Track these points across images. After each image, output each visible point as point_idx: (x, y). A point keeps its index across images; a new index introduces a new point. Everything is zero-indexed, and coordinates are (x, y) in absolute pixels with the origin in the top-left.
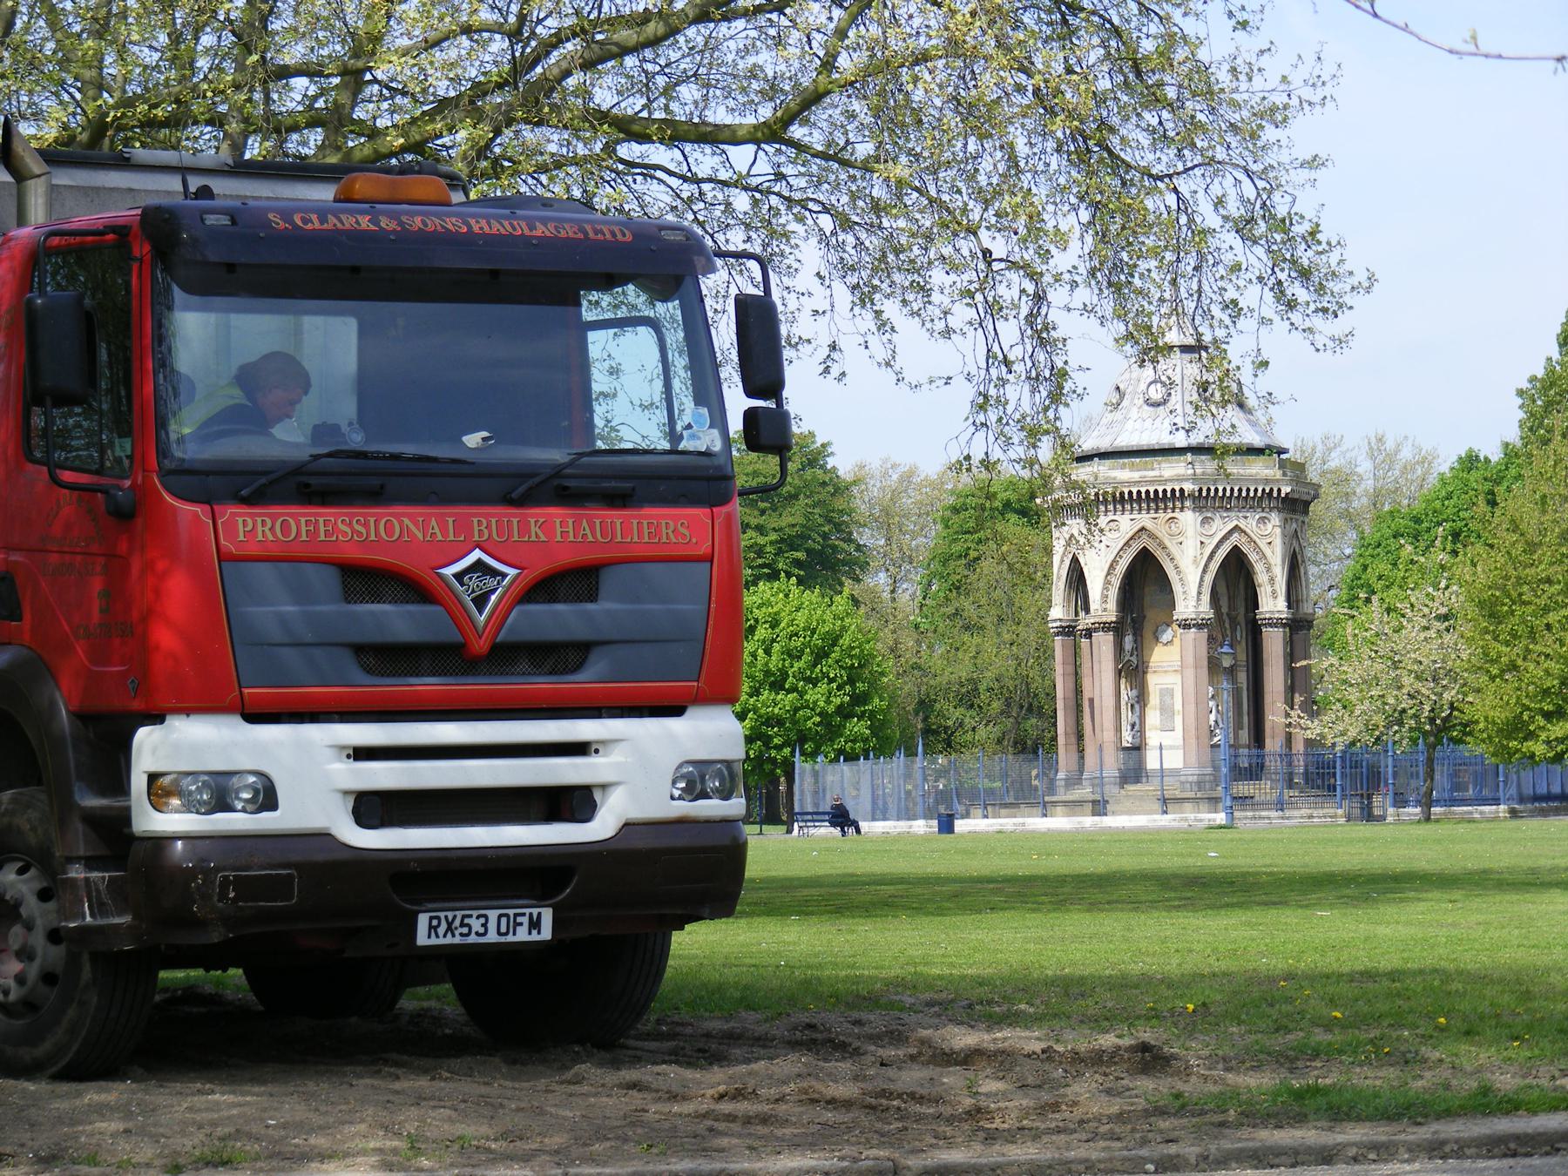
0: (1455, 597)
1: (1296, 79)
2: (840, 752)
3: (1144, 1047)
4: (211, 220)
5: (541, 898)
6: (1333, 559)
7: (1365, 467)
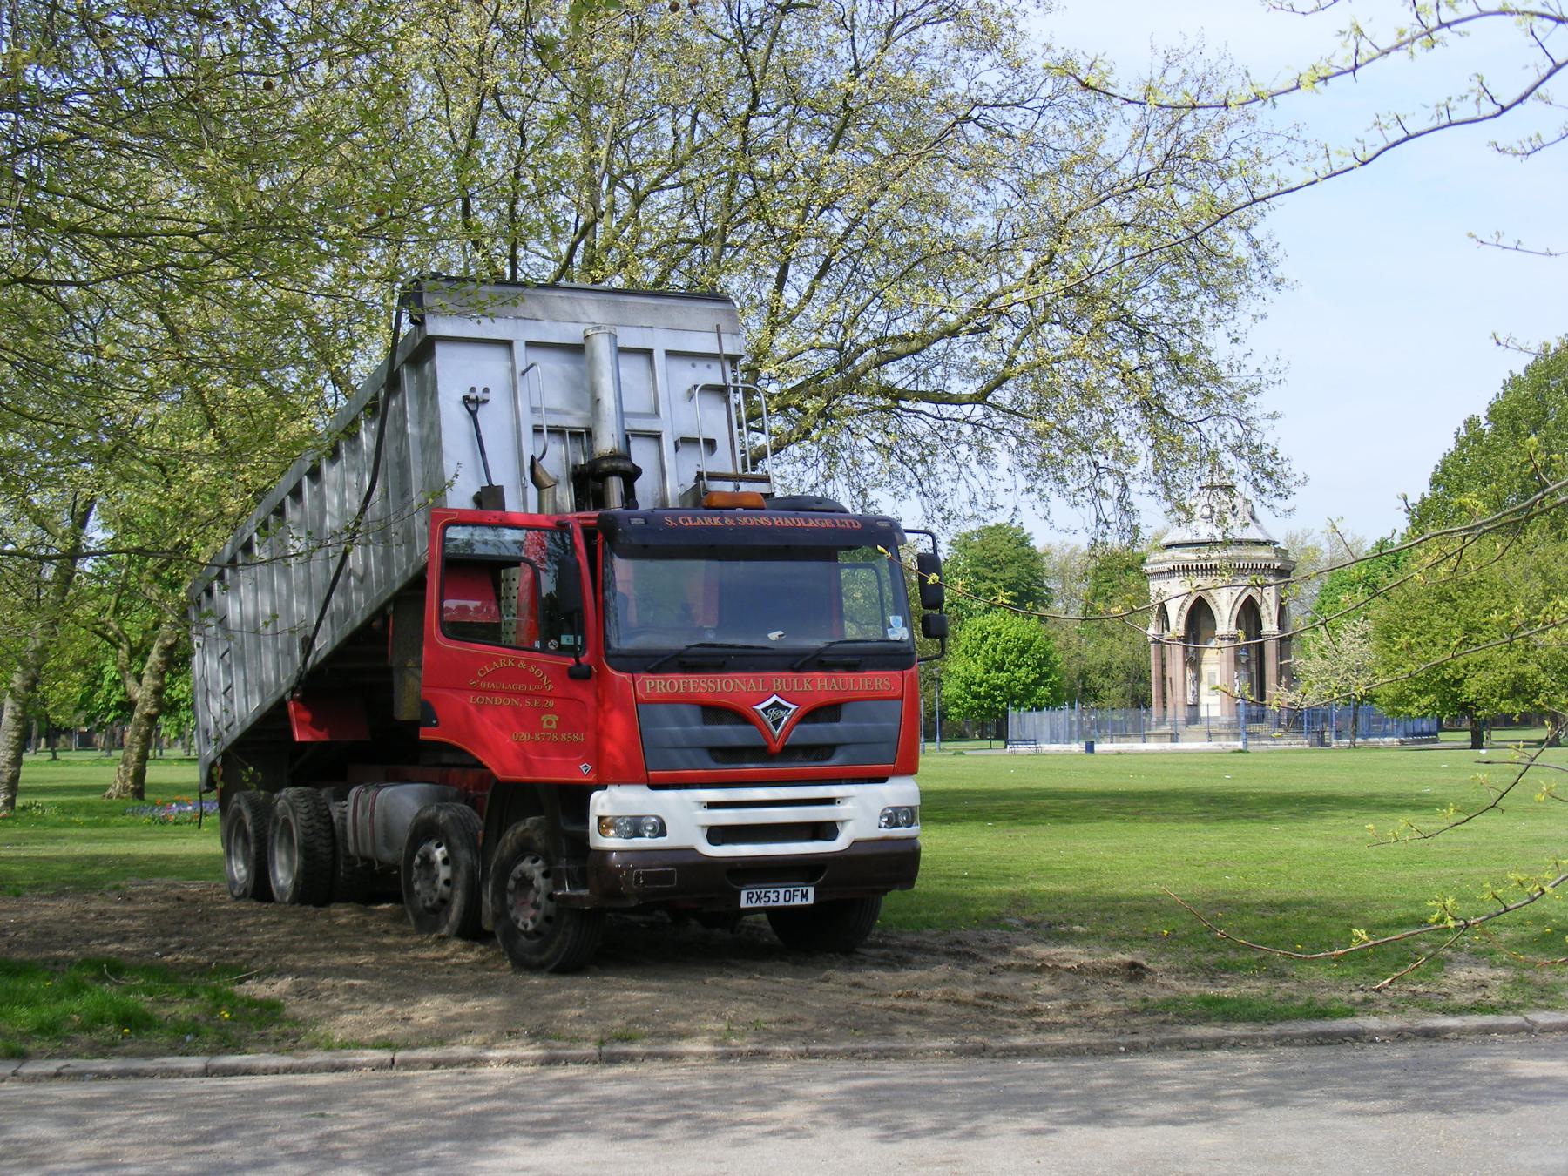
0: (1369, 627)
1: (1265, 370)
2: (1034, 705)
3: (1133, 965)
4: (634, 521)
5: (808, 882)
6: (1307, 593)
7: (1325, 546)
